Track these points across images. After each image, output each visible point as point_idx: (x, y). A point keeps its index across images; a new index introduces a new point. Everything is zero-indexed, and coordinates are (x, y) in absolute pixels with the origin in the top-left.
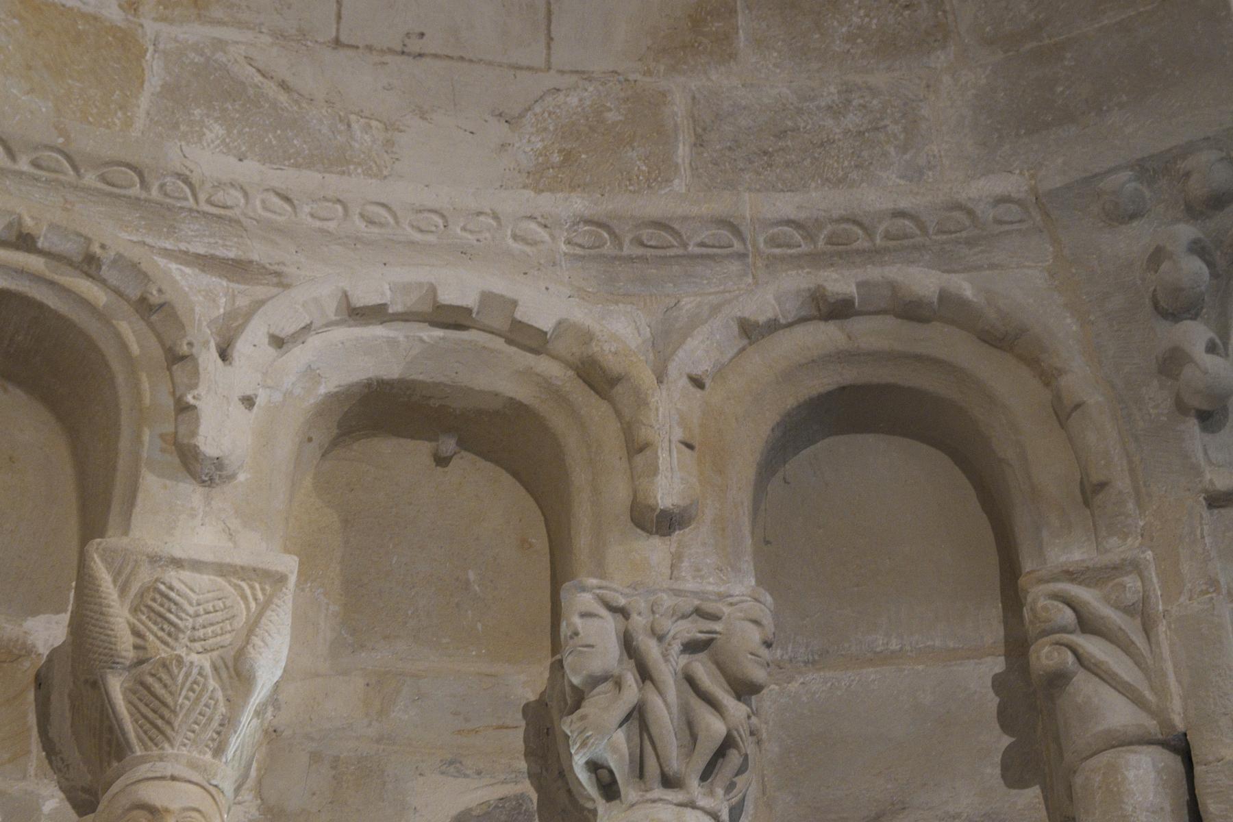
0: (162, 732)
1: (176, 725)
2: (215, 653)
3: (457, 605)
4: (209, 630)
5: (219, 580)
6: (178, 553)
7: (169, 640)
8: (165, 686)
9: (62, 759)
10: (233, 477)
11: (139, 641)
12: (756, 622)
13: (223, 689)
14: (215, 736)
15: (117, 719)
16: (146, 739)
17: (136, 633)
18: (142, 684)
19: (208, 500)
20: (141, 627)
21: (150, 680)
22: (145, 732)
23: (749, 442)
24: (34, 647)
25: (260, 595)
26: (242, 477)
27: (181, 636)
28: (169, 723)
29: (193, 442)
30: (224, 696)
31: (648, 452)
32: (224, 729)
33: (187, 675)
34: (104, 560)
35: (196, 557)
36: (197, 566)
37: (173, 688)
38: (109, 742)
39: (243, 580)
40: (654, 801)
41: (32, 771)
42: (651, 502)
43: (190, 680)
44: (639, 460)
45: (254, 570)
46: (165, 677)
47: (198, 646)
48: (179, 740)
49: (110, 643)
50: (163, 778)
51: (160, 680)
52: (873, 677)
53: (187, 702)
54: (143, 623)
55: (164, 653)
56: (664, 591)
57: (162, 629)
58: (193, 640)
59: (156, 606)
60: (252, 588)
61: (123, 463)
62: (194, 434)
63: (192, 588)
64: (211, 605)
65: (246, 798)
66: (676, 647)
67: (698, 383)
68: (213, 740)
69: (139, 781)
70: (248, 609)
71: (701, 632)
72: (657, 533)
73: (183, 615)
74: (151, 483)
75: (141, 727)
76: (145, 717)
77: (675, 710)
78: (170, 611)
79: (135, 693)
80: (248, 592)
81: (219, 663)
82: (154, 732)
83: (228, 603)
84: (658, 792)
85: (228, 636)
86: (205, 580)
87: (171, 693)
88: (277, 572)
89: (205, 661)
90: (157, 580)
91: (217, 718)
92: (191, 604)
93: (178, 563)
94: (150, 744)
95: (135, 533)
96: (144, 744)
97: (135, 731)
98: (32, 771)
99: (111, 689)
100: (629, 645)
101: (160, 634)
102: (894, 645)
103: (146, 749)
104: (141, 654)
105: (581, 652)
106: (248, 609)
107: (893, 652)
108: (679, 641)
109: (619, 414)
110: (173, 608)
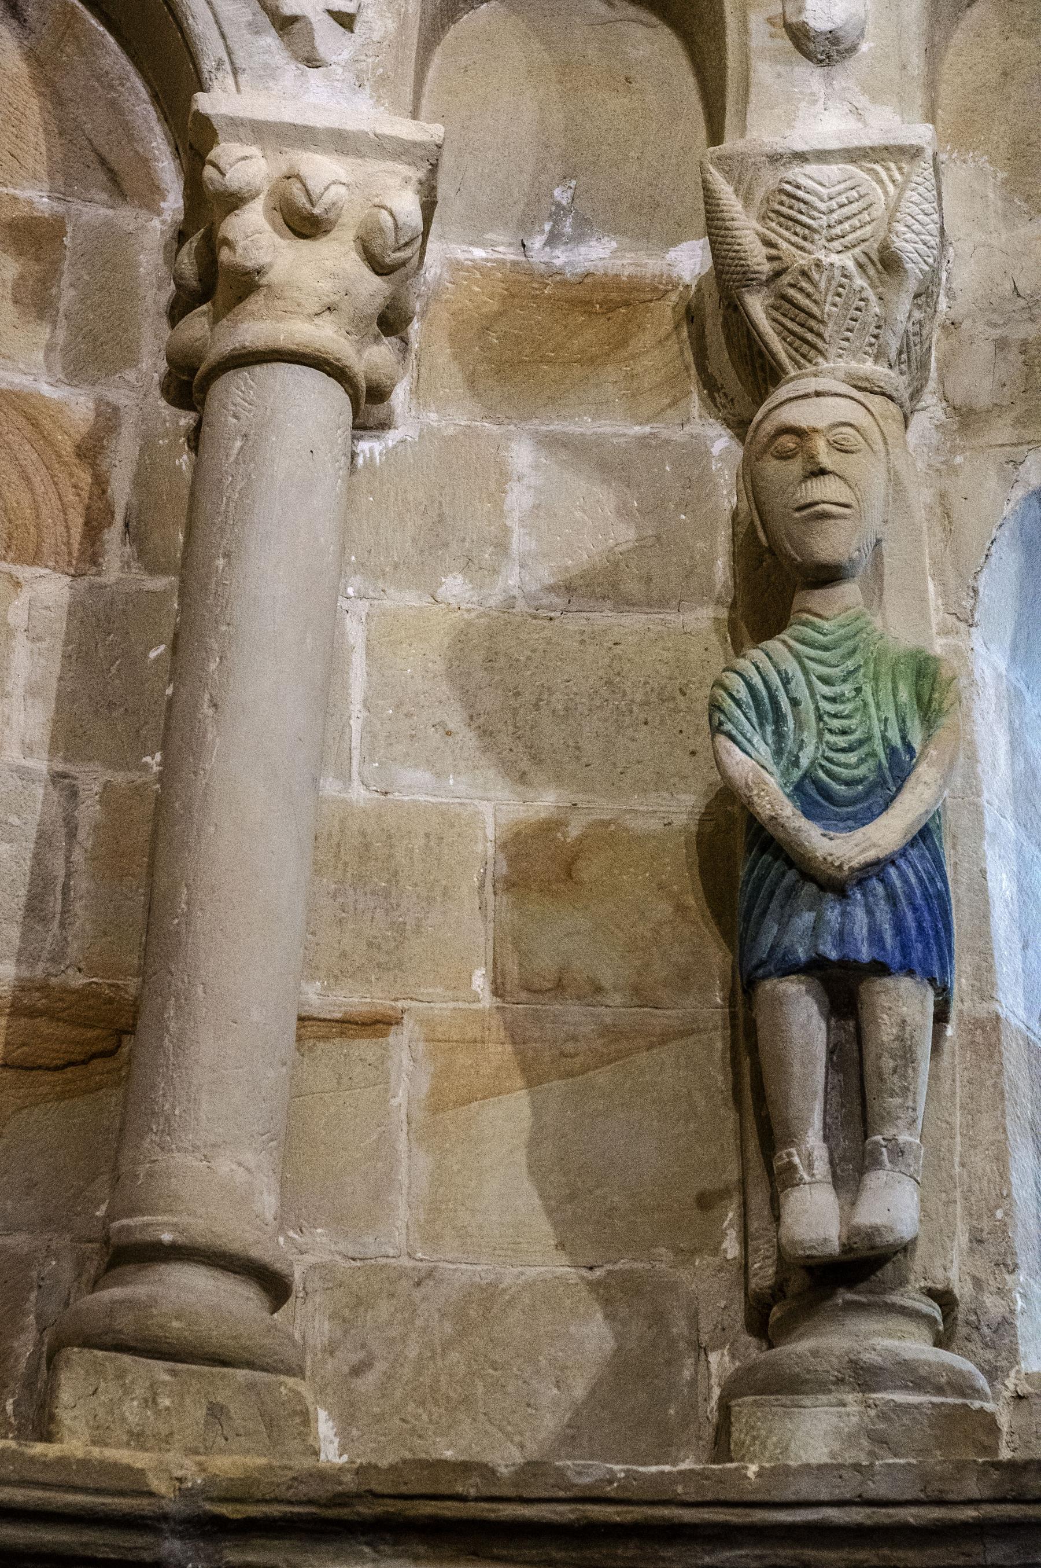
0: (813, 346)
1: (826, 336)
2: (857, 250)
4: (846, 226)
5: (850, 167)
6: (800, 147)
7: (805, 244)
8: (808, 296)
9: (725, 394)
10: (853, 49)
11: (773, 252)
13: (873, 286)
14: (873, 340)
15: (762, 341)
16: (798, 357)
17: (768, 244)
18: (784, 297)
19: (828, 79)
20: (773, 236)
21: (791, 292)
25: (897, 176)
26: (864, 47)
27: (816, 237)
28: (819, 335)
30: (876, 294)
33: (830, 279)
34: (721, 170)
35: (819, 147)
36: (823, 156)
37: (816, 296)
38: (763, 370)
41: (695, 412)
43: (834, 283)
45: (886, 148)
46: (804, 284)
47: (837, 245)
48: (833, 351)
49: (741, 259)
51: (801, 290)
53: (834, 309)
55: (802, 260)
57: (796, 234)
58: (831, 240)
59: (787, 210)
60: (887, 169)
61: (732, 61)
62: (801, 10)
63: (819, 180)
65: (929, 402)
68: (871, 345)
69: (782, 404)
70: (886, 193)
73: (815, 214)
74: (763, 72)
75: (790, 344)
76: (792, 333)
78: (801, 213)
79: (776, 308)
80: (884, 175)
81: (863, 259)
82: (805, 349)
83: (862, 190)
85: (868, 228)
86: (833, 171)
87: (815, 302)
88: (912, 146)
89: (847, 261)
92: (822, 200)
93: (801, 157)
94: (802, 361)
95: (752, 134)
96: (797, 362)
98: (695, 412)
99: (751, 311)
101: (794, 239)
104: (776, 265)
106: (886, 193)
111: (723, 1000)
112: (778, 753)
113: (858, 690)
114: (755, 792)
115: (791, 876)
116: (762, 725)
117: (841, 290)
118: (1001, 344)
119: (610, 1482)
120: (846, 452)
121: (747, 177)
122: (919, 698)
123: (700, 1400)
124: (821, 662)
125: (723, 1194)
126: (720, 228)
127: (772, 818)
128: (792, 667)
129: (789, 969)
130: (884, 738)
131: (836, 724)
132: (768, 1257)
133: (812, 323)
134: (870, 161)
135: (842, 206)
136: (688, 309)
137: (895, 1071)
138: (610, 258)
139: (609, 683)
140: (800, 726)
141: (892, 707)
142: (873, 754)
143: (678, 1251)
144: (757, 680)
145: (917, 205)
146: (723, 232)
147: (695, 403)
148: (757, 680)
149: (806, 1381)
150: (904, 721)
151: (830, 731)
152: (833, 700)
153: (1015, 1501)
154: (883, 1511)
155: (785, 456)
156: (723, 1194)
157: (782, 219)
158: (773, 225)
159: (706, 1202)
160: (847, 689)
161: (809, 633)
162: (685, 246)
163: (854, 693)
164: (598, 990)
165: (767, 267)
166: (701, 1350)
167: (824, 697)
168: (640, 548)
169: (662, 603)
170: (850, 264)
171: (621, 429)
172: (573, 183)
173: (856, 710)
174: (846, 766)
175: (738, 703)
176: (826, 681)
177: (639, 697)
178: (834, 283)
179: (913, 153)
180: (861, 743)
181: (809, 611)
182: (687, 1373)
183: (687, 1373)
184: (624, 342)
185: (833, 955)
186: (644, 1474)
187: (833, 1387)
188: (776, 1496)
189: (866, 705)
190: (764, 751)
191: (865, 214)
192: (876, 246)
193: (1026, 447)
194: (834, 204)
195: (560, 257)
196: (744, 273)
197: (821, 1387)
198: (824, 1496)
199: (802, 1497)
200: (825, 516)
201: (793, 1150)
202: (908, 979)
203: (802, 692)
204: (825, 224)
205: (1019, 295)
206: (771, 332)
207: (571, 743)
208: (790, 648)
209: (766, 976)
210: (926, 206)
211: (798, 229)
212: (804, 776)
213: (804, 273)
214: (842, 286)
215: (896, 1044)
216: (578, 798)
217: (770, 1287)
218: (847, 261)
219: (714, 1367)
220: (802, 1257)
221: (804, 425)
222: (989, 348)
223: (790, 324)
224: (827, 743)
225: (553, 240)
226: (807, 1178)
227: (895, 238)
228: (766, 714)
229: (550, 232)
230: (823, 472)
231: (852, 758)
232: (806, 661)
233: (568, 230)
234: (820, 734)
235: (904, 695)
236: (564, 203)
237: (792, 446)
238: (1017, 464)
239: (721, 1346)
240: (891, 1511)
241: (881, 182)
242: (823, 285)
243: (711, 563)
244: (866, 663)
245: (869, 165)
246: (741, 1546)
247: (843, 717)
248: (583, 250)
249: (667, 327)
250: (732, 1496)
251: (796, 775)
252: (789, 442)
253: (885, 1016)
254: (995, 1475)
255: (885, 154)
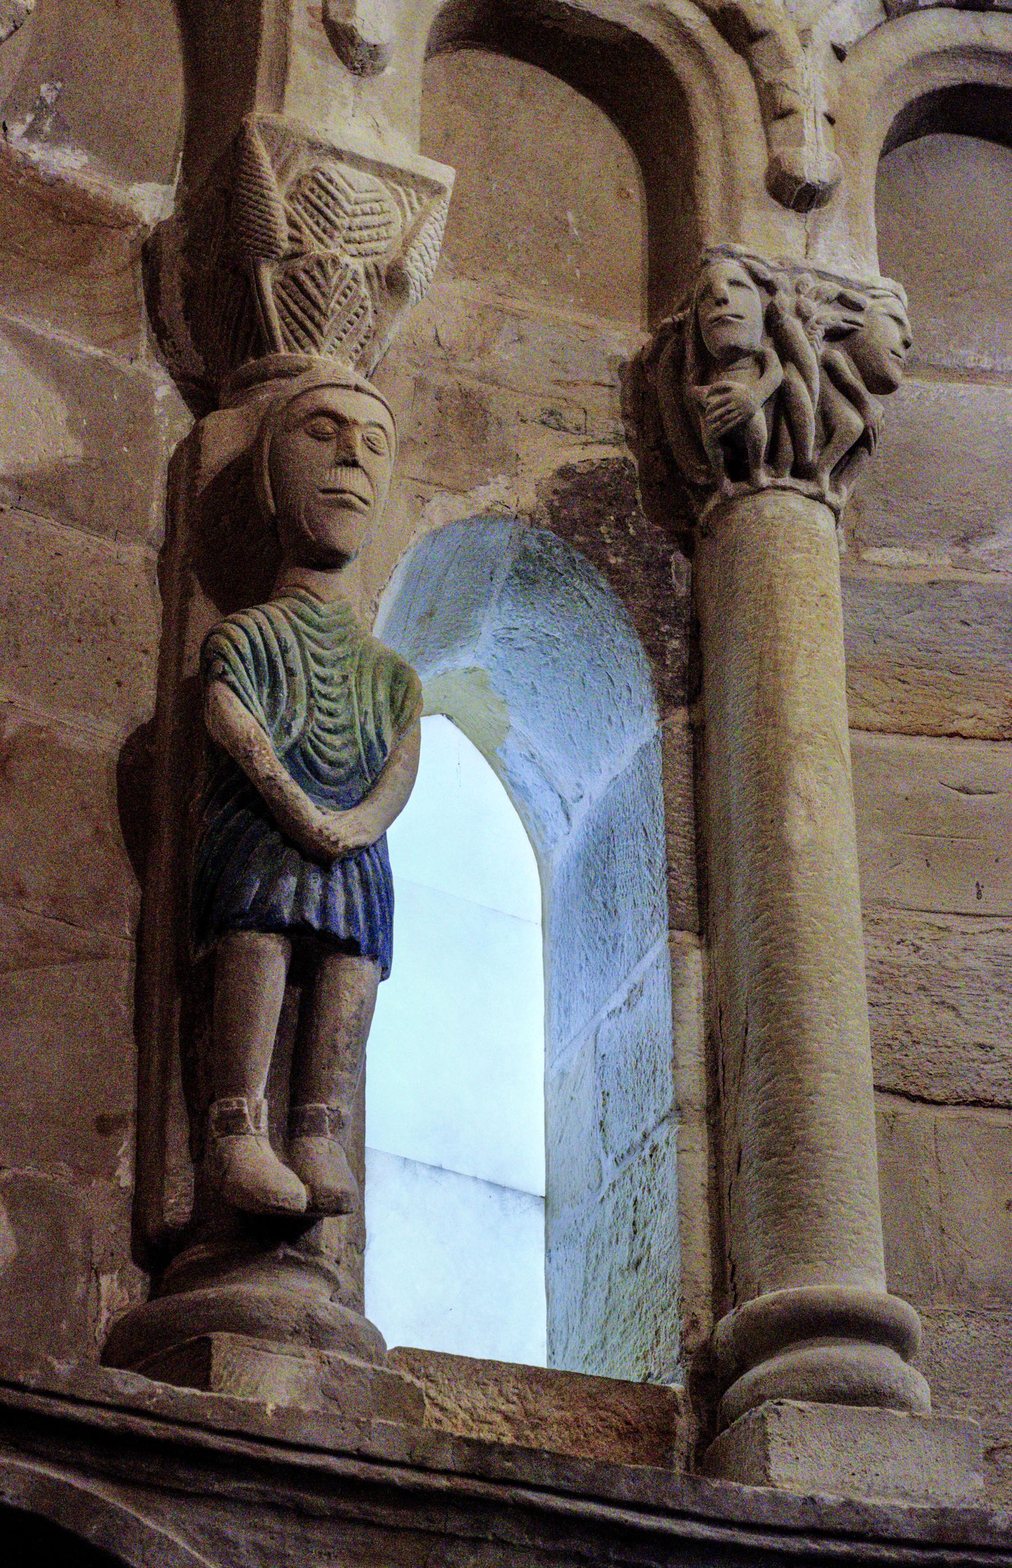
1: (326, 329)
2: (369, 260)
3: (556, 246)
4: (365, 233)
5: (377, 180)
11: (296, 233)
12: (898, 321)
13: (373, 299)
14: (359, 348)
16: (291, 338)
17: (293, 224)
18: (295, 279)
20: (298, 219)
21: (303, 277)
22: (292, 332)
23: (876, 126)
24: (141, 215)
27: (336, 234)
28: (318, 326)
29: (349, 22)
30: (373, 306)
31: (791, 119)
32: (368, 343)
33: (341, 279)
37: (326, 290)
39: (400, 184)
40: (784, 488)
41: (143, 351)
42: (797, 173)
43: (344, 283)
44: (779, 127)
46: (317, 273)
47: (352, 248)
48: (326, 346)
49: (270, 229)
50: (347, 387)
51: (313, 278)
52: (962, 393)
53: (338, 307)
54: (298, 213)
55: (317, 250)
56: (809, 271)
57: (318, 224)
59: (317, 198)
60: (408, 195)
61: (268, 32)
62: (349, 14)
63: (354, 184)
64: (368, 205)
66: (820, 333)
67: (839, 53)
68: (357, 351)
69: (323, 386)
71: (845, 321)
72: (793, 208)
73: (341, 213)
77: (817, 397)
79: (284, 287)
82: (300, 333)
83: (386, 206)
84: (787, 480)
86: (364, 179)
87: (324, 295)
89: (357, 265)
90: (315, 169)
91: (364, 329)
92: (350, 203)
93: (338, 154)
94: (295, 344)
97: (281, 326)
100: (772, 322)
101: (315, 228)
102: (986, 363)
103: (290, 350)
104: (296, 247)
105: (730, 322)
107: (983, 371)
108: (823, 327)
109: (755, 73)
110: (331, 202)
111: (132, 933)
112: (272, 715)
113: (345, 678)
114: (257, 748)
115: (274, 838)
116: (260, 685)
117: (348, 291)
118: (420, 385)
119: (151, 1396)
120: (375, 452)
121: (287, 152)
122: (392, 701)
123: (90, 1320)
124: (315, 641)
125: (120, 1121)
126: (256, 193)
127: (269, 778)
128: (290, 639)
129: (270, 924)
130: (363, 731)
131: (325, 704)
132: (186, 1195)
133: (316, 314)
134: (395, 182)
135: (364, 214)
136: (144, 246)
137: (348, 1046)
138: (80, 171)
139: (49, 591)
140: (293, 696)
141: (371, 702)
142: (354, 743)
143: (77, 1169)
144: (259, 640)
145: (432, 239)
146: (257, 197)
147: (144, 342)
148: (259, 640)
149: (265, 1327)
150: (380, 719)
151: (320, 709)
152: (323, 680)
153: (482, 1478)
154: (377, 1468)
155: (319, 436)
156: (120, 1121)
157: (308, 205)
158: (299, 208)
159: (105, 1126)
160: (336, 673)
161: (306, 609)
162: (153, 186)
163: (341, 680)
164: (21, 893)
165: (286, 245)
166: (95, 1272)
167: (317, 676)
168: (85, 466)
169: (102, 529)
170: (361, 271)
171: (80, 346)
172: (59, 85)
173: (342, 695)
174: (332, 747)
175: (243, 660)
176: (319, 660)
177: (75, 612)
178: (344, 283)
179: (437, 190)
180: (344, 728)
181: (307, 589)
182: (79, 1290)
183: (79, 1290)
184: (85, 259)
185: (316, 924)
186: (178, 1394)
187: (289, 1338)
188: (290, 1437)
189: (350, 694)
190: (261, 713)
191: (383, 230)
192: (386, 262)
193: (433, 488)
194: (358, 209)
195: (37, 152)
196: (270, 244)
197: (279, 1335)
198: (329, 1444)
199: (311, 1441)
200: (348, 505)
201: (245, 1100)
202: (370, 964)
203: (298, 666)
204: (347, 225)
205: (439, 345)
206: (273, 306)
207: (12, 639)
208: (288, 618)
209: (248, 928)
210: (437, 243)
211: (322, 221)
212: (295, 745)
213: (320, 264)
214: (349, 288)
215: (354, 1022)
216: (16, 696)
217: (185, 1225)
218: (357, 265)
219: (104, 1289)
220: (273, 1207)
221: (346, 415)
222: (410, 383)
223: (294, 308)
224: (317, 720)
225: (32, 133)
226: (253, 1130)
227: (408, 262)
228: (265, 677)
229: (32, 125)
230: (355, 464)
231: (337, 740)
232: (305, 638)
233: (47, 129)
234: (310, 709)
235: (382, 695)
236: (49, 101)
237: (329, 429)
238: (425, 501)
239: (112, 1271)
240: (384, 1469)
241: (400, 203)
242: (334, 281)
243: (147, 501)
244: (353, 654)
245: (396, 186)
246: (247, 1478)
247: (330, 700)
248: (58, 154)
249: (123, 260)
250: (251, 1429)
251: (288, 742)
252: (328, 426)
253: (347, 994)
254: (466, 1450)
255: (410, 182)
